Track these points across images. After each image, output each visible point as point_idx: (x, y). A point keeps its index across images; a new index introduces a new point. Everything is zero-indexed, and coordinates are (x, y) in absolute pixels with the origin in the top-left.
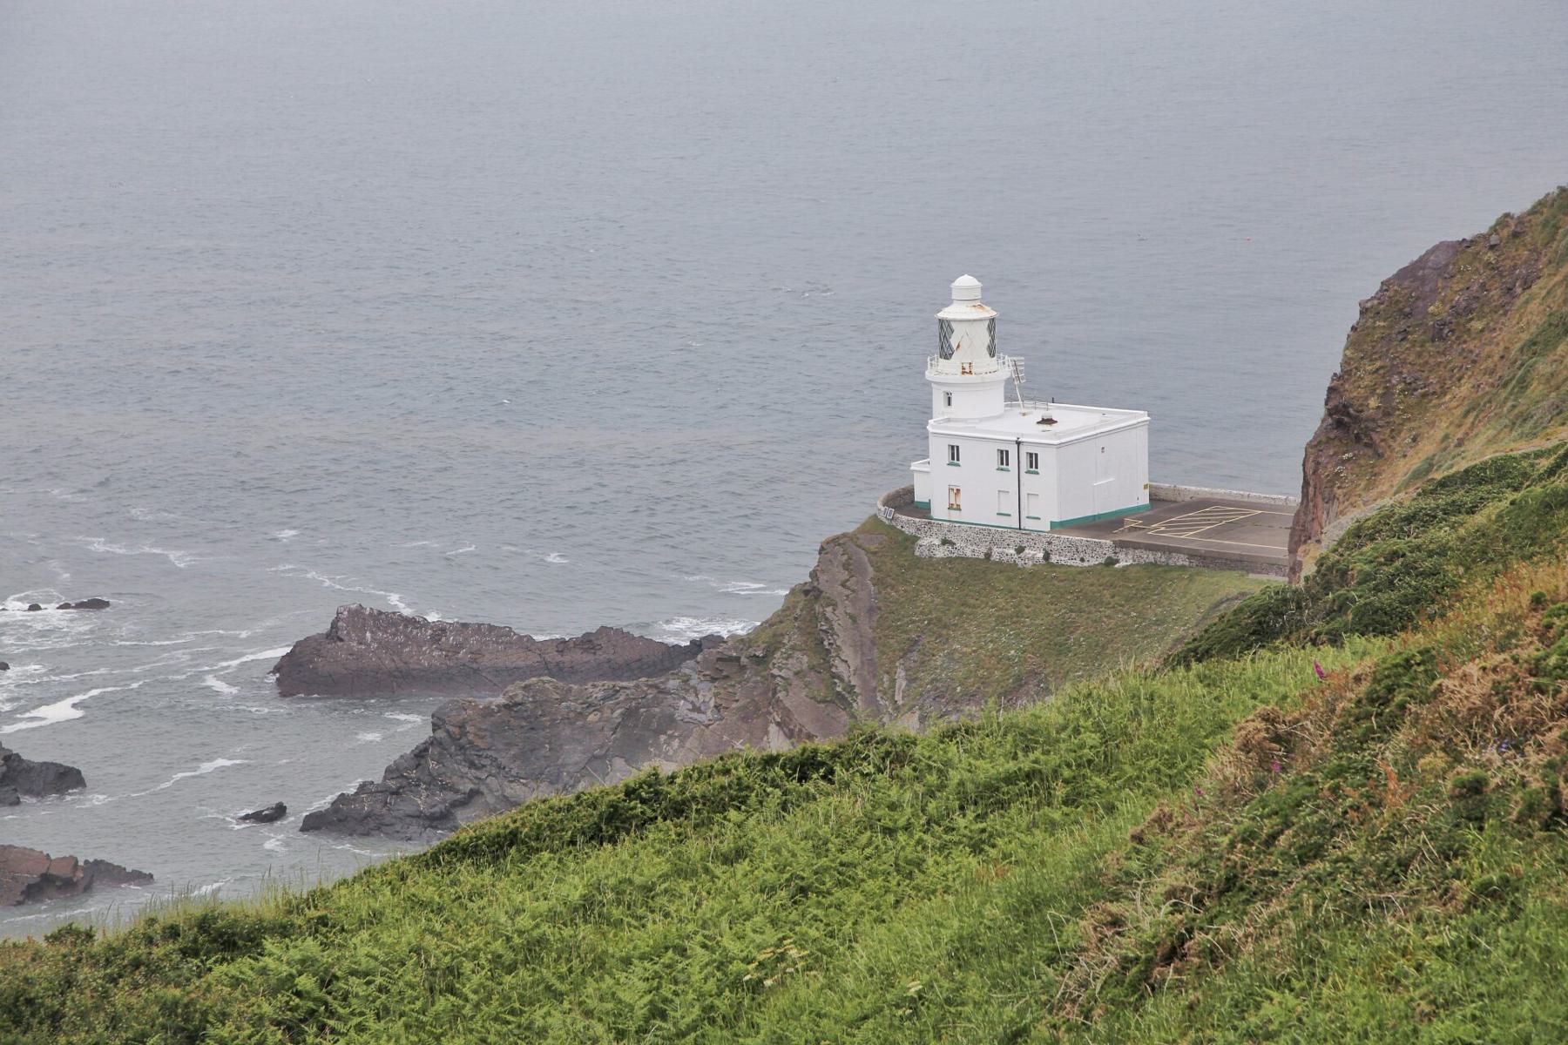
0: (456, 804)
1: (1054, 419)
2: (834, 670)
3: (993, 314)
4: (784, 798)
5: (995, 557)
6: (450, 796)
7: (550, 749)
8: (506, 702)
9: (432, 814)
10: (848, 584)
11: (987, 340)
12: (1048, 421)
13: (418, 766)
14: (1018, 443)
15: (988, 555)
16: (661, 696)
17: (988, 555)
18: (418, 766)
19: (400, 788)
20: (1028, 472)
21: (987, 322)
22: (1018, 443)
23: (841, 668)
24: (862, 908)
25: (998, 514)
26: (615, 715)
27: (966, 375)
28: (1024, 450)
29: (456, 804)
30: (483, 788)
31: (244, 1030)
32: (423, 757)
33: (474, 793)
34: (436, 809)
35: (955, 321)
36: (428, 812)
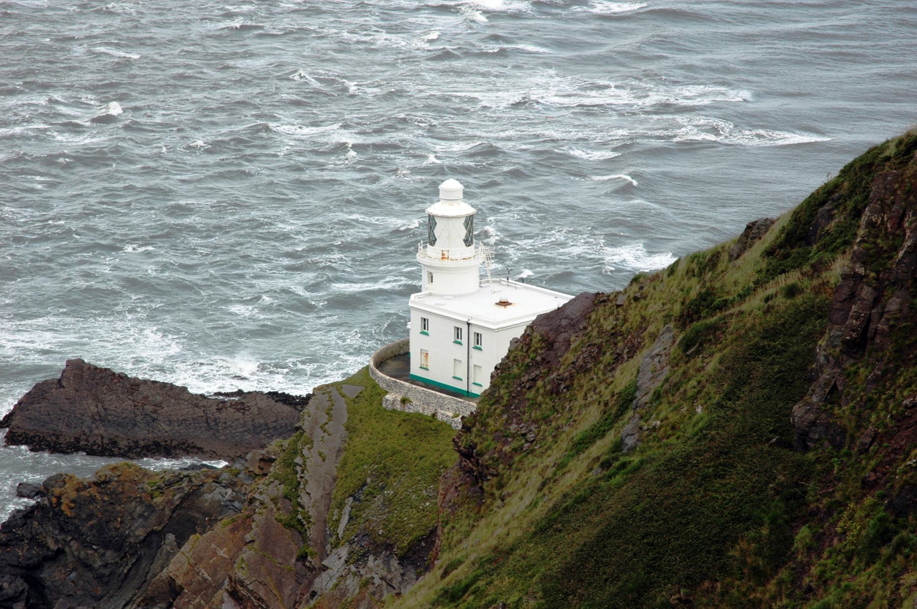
0: (46, 559)
1: (510, 301)
2: (299, 500)
3: (471, 211)
4: (476, 524)
5: (439, 417)
6: (43, 552)
7: (121, 522)
8: (96, 480)
9: (27, 565)
10: (326, 426)
11: (464, 232)
12: (504, 304)
13: (24, 525)
14: (469, 324)
15: (434, 415)
16: (214, 484)
17: (434, 415)
18: (24, 525)
19: (9, 541)
20: (475, 348)
21: (463, 220)
22: (469, 324)
23: (304, 500)
24: (843, 584)
25: (454, 377)
26: (176, 498)
27: (445, 260)
28: (473, 330)
29: (46, 559)
30: (67, 549)
31: (222, 598)
32: (30, 518)
33: (60, 552)
34: (31, 561)
35: (438, 216)
36: (24, 563)
